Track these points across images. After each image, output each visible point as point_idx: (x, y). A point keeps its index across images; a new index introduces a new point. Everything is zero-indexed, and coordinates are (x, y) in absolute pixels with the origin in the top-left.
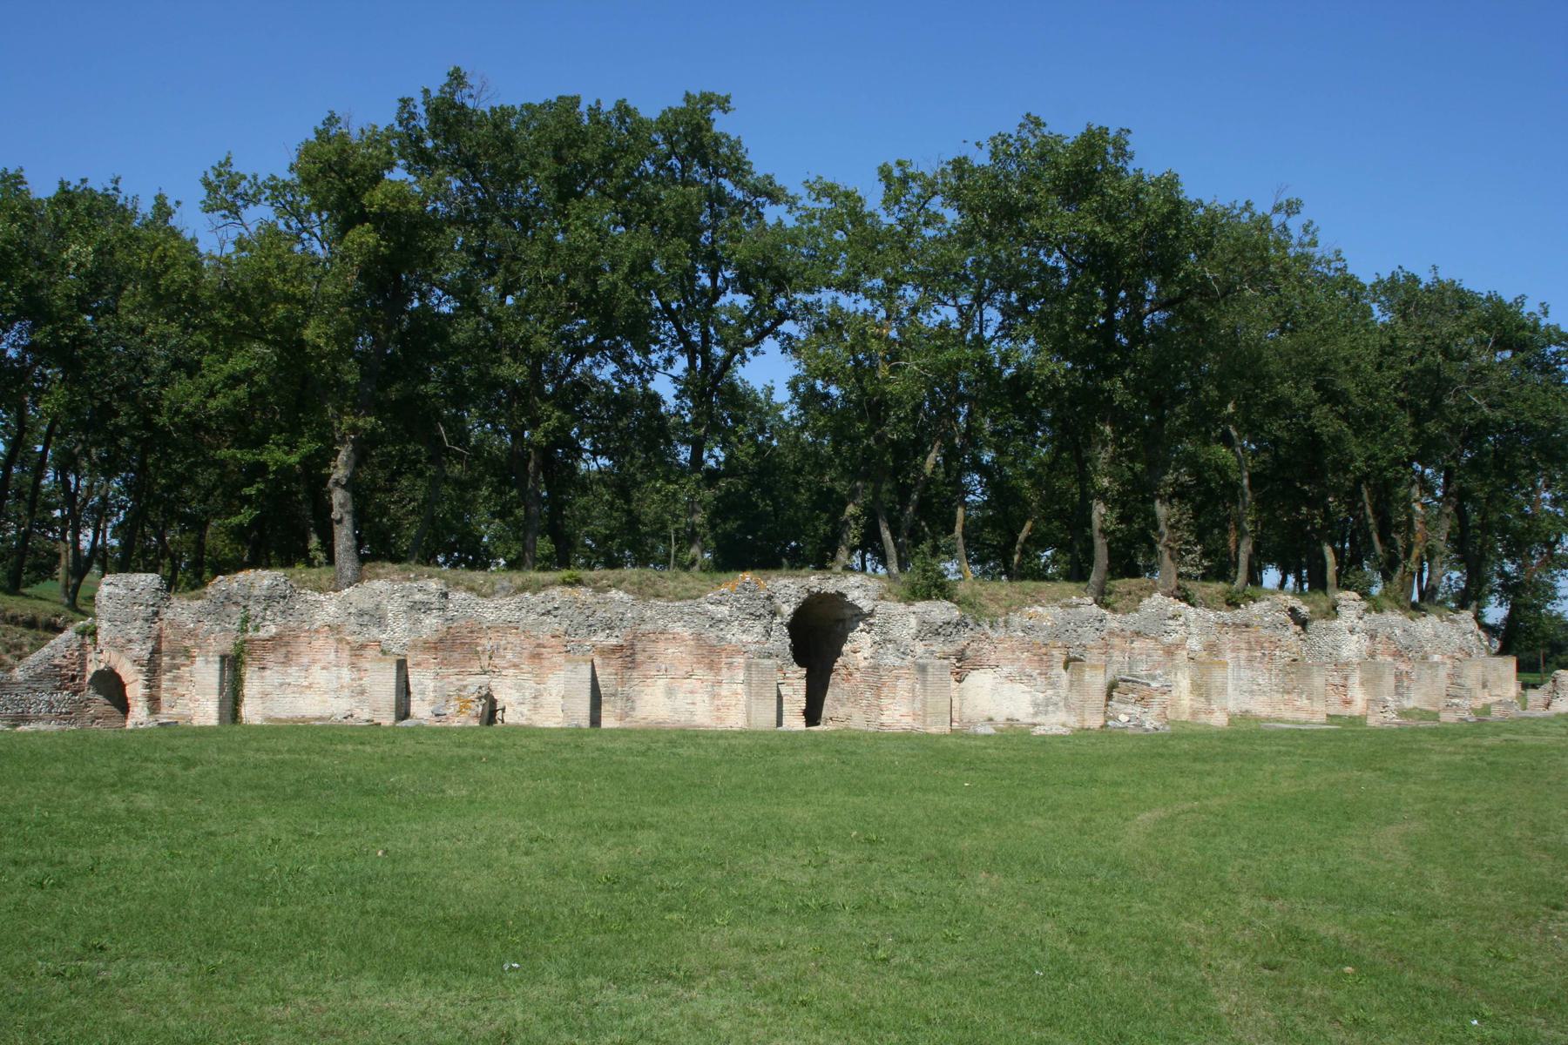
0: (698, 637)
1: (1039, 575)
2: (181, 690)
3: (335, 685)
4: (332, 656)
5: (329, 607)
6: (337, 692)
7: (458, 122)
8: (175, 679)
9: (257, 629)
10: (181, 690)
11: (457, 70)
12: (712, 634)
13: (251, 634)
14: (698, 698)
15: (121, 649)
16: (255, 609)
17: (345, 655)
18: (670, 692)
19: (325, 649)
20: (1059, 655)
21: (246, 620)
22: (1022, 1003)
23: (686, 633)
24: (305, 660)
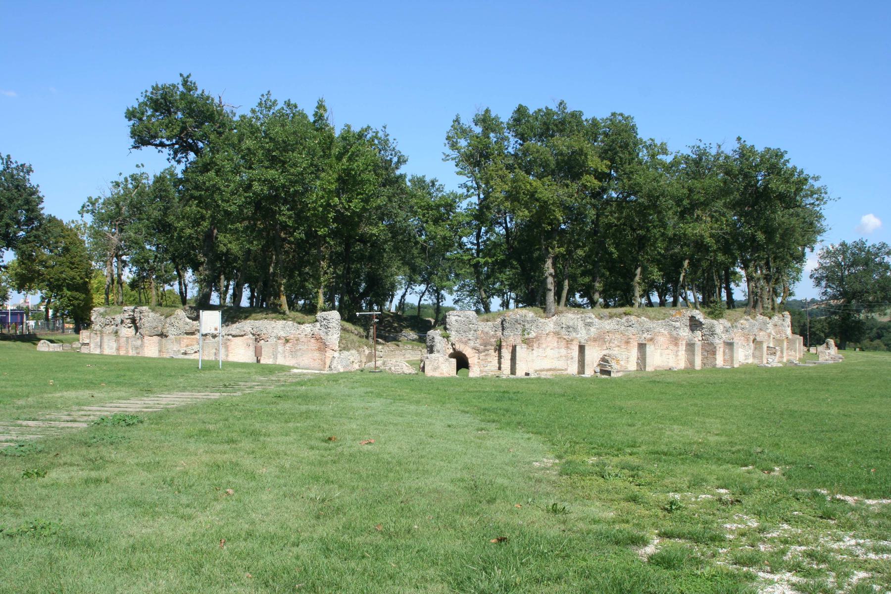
0: (670, 334)
1: (562, 312)
2: (489, 360)
3: (557, 355)
4: (556, 344)
5: (550, 324)
6: (559, 358)
7: (653, 156)
8: (486, 355)
9: (528, 334)
10: (489, 360)
11: (521, 107)
12: (674, 333)
13: (527, 336)
14: (670, 357)
15: (466, 343)
16: (527, 326)
17: (563, 343)
18: (661, 355)
19: (552, 341)
20: (752, 338)
21: (524, 331)
22: (234, 528)
23: (666, 332)
24: (544, 346)
